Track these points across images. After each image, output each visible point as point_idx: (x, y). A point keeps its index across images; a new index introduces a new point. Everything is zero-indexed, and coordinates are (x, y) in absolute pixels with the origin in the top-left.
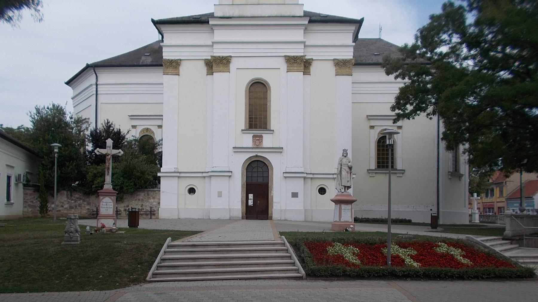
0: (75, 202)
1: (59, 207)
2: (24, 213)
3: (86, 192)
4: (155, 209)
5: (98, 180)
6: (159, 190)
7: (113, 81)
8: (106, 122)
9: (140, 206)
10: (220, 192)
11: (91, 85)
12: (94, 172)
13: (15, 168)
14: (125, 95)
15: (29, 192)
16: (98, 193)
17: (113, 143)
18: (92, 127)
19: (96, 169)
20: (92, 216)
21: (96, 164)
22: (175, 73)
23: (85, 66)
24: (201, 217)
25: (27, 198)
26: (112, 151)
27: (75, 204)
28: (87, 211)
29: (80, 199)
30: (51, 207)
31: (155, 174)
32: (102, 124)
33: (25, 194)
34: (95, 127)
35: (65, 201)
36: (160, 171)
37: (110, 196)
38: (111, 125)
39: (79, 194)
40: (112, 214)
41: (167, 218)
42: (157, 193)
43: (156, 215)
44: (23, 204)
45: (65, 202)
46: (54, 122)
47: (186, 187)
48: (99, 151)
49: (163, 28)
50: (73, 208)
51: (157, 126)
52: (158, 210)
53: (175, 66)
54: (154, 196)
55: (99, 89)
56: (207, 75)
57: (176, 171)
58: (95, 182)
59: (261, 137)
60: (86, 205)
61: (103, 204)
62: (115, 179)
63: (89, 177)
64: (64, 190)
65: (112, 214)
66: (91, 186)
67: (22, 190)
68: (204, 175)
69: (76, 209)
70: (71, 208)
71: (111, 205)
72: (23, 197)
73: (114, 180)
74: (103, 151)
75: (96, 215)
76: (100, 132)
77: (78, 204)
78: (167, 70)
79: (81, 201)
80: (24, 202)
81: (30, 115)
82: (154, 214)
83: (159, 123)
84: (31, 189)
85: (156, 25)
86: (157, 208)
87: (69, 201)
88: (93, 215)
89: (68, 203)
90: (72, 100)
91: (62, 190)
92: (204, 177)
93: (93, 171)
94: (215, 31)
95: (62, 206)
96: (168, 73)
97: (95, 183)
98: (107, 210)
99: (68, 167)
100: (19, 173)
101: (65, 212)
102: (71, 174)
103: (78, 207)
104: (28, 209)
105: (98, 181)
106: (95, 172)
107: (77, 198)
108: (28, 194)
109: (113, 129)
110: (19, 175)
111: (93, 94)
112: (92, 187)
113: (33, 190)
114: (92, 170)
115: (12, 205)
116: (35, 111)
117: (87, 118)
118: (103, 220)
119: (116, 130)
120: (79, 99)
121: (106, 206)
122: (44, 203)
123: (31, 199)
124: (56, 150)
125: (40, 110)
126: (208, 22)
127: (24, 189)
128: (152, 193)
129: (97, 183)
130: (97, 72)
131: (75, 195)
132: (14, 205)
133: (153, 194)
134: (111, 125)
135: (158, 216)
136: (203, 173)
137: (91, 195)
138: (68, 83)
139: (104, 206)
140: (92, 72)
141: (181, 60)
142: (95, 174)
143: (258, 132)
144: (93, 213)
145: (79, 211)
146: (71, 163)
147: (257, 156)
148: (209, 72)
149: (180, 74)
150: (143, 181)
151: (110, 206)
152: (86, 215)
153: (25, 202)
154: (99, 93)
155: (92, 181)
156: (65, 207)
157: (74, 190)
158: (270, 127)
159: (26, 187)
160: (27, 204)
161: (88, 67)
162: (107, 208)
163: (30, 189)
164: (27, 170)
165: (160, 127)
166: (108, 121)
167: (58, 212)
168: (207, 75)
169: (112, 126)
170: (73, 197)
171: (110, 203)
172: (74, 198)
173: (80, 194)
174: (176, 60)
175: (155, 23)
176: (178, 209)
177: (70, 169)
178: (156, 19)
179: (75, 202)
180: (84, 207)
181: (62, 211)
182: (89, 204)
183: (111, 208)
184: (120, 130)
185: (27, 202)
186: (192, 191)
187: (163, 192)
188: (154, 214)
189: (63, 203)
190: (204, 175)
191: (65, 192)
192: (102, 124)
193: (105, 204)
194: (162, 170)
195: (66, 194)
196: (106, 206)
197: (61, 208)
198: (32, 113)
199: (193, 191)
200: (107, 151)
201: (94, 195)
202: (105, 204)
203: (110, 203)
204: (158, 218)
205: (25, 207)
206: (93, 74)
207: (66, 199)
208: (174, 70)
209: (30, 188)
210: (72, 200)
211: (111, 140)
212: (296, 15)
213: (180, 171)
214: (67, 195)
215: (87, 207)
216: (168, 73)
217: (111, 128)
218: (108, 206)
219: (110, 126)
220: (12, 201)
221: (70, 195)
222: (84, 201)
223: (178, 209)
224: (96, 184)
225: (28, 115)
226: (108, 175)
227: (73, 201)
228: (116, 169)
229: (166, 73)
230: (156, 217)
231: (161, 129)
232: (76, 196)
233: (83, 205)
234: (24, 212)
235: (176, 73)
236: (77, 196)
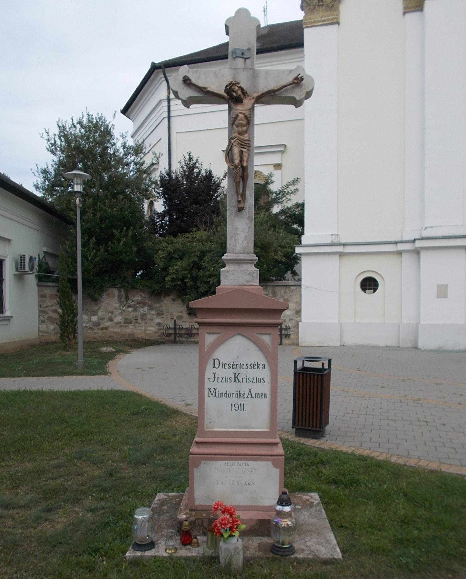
0: (135, 310)
1: (106, 320)
2: (41, 334)
3: (155, 290)
4: (290, 325)
5: (176, 265)
6: (297, 283)
8: (187, 158)
10: (443, 285)
11: (160, 102)
12: (169, 249)
13: (12, 241)
14: (217, 112)
15: (47, 291)
18: (162, 168)
19: (172, 243)
20: (167, 338)
21: (170, 234)
22: (329, 20)
24: (392, 342)
25: (45, 305)
27: (135, 314)
28: (157, 327)
29: (144, 304)
30: (91, 321)
31: (289, 250)
32: (180, 162)
33: (42, 296)
34: (167, 168)
35: (116, 308)
36: (301, 243)
37: (254, 332)
38: (196, 163)
39: (142, 294)
40: (265, 429)
41: (317, 345)
42: (292, 291)
43: (292, 337)
44: (39, 316)
45: (115, 311)
46: (82, 133)
47: (357, 277)
48: (194, 80)
50: (131, 323)
51: (272, 166)
52: (297, 326)
53: (330, 5)
54: (286, 297)
55: (172, 108)
56: (404, 13)
57: (336, 241)
58: (171, 270)
60: (154, 316)
61: (221, 372)
62: (208, 263)
63: (160, 258)
64: (114, 286)
65: (265, 429)
66: (164, 279)
67: (36, 288)
68: (400, 247)
69: (137, 325)
70: (128, 322)
71: (260, 380)
72: (39, 303)
73: (207, 265)
75: (173, 336)
76: (177, 178)
77: (140, 313)
78: (313, 16)
79: (146, 308)
80: (40, 312)
81: (47, 138)
82: (288, 336)
83: (276, 159)
84: (55, 286)
86: (293, 322)
87: (124, 308)
88: (168, 335)
89: (121, 313)
91: (109, 287)
92: (400, 253)
93: (167, 247)
95: (111, 320)
96: (315, 22)
97: (170, 272)
98: (241, 407)
99: (119, 241)
100: (22, 253)
101: (116, 330)
102: (124, 254)
103: (140, 321)
104: (47, 327)
105: (176, 267)
106: (170, 248)
107: (138, 303)
108: (48, 295)
109: (199, 172)
110: (22, 258)
111: (164, 118)
112: (165, 280)
113: (56, 288)
114: (165, 245)
115: (9, 320)
116: (57, 131)
118: (221, 464)
119: (203, 173)
121: (232, 387)
122: (68, 316)
123: (52, 306)
124: (78, 188)
125: (68, 130)
127: (38, 286)
128: (282, 292)
129: (174, 271)
131: (134, 297)
132: (12, 320)
133: (285, 293)
134: (196, 163)
135: (298, 339)
136: (396, 243)
137: (164, 297)
139: (222, 387)
140: (161, 78)
142: (170, 253)
144: (167, 332)
145: (143, 329)
146: (123, 233)
148: (409, 5)
149: (341, 21)
150: (265, 266)
151: (257, 388)
152: (156, 337)
153: (42, 312)
154: (172, 114)
155: (165, 269)
156: (116, 320)
157: (133, 288)
159: (42, 281)
160: (46, 317)
161: (155, 68)
162: (239, 395)
163: (50, 286)
164: (45, 249)
166: (190, 155)
167: (104, 331)
168: (404, 13)
169: (197, 165)
170: (130, 302)
171: (255, 366)
172: (133, 303)
173: (144, 295)
176: (341, 325)
177: (122, 243)
179: (135, 310)
180: (152, 320)
181: (111, 330)
182: (160, 314)
183: (258, 395)
184: (210, 171)
185: (45, 312)
187: (307, 288)
188: (288, 336)
189: (112, 313)
190: (400, 247)
191: (116, 291)
192: (180, 162)
193: (229, 373)
194: (304, 240)
195: (117, 294)
196: (232, 387)
197: (109, 324)
198: (51, 134)
199: (370, 285)
201: (169, 295)
203: (255, 366)
204: (298, 345)
205: (43, 322)
206: (163, 81)
207: (117, 305)
208: (328, 13)
209: (49, 284)
210: (129, 306)
213: (343, 241)
214: (120, 297)
215: (157, 321)
216: (315, 22)
217: (196, 170)
218: (244, 388)
219: (194, 167)
220: (8, 313)
221: (124, 296)
222: (151, 308)
223: (341, 325)
224: (172, 273)
225: (42, 137)
226: (240, 210)
227: (130, 309)
228: (209, 244)
229: (311, 23)
230: (290, 341)
231: (280, 171)
232: (136, 298)
233: (149, 317)
234: (41, 332)
235: (332, 19)
236: (138, 298)
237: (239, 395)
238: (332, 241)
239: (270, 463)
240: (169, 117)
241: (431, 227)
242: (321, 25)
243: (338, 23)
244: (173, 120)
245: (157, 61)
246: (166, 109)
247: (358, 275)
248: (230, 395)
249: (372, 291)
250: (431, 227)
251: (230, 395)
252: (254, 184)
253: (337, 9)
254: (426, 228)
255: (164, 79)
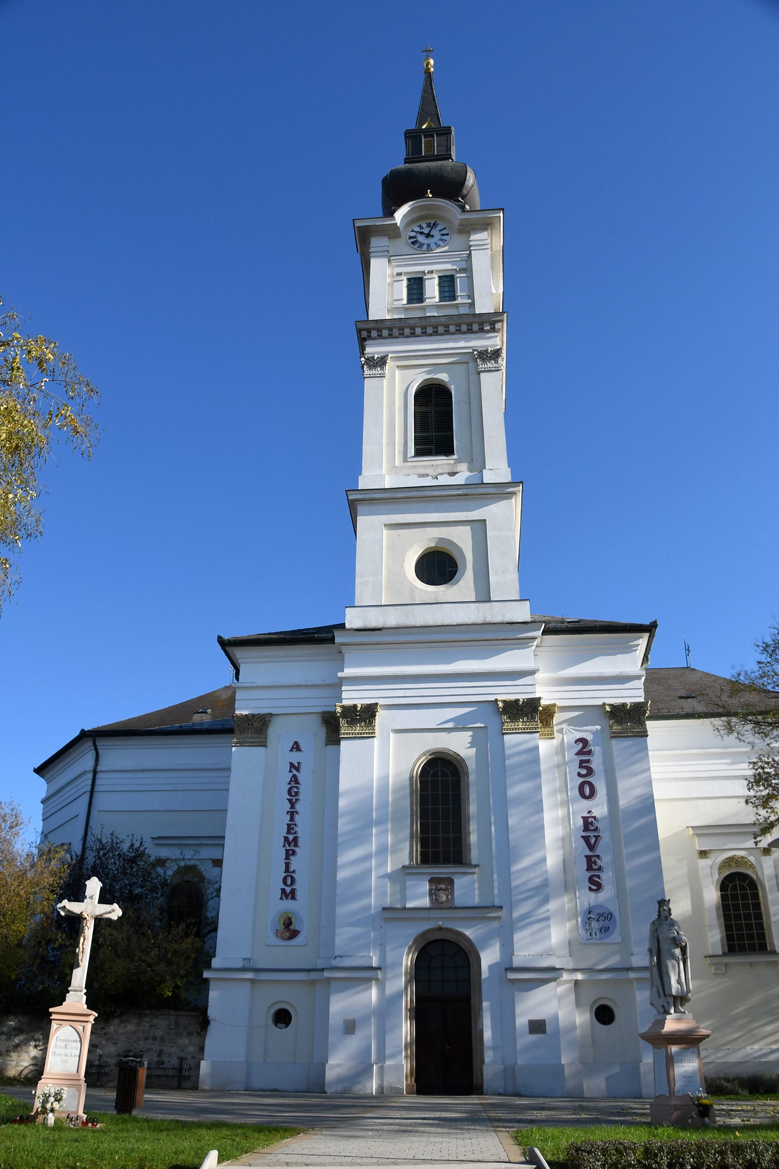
7: (130, 765)
9: (156, 1054)
11: (85, 773)
16: (50, 1014)
17: (101, 888)
23: (76, 733)
26: (95, 906)
37: (73, 1024)
49: (239, 653)
55: (98, 782)
56: (326, 745)
59: (451, 882)
74: (75, 907)
85: (227, 648)
90: (42, 805)
94: (346, 656)
111: (86, 792)
117: (65, 842)
120: (57, 801)
121: (63, 1051)
126: (332, 640)
130: (98, 747)
138: (40, 771)
139: (58, 1051)
141: (271, 715)
143: (442, 871)
147: (440, 929)
154: (97, 789)
158: (470, 860)
161: (84, 735)
162: (66, 1055)
165: (218, 863)
168: (326, 745)
173: (22, 1020)
174: (262, 715)
175: (224, 644)
178: (226, 637)
186: (282, 1017)
193: (63, 1044)
194: (215, 963)
196: (63, 1051)
200: (86, 908)
202: (63, 1044)
211: (98, 880)
212: (515, 620)
237: (66, 1055)
238: (244, 965)
239: (75, 1089)
240: (95, 772)
241: (341, 957)
242: (248, 746)
243: (266, 746)
244: (95, 795)
245: (87, 728)
246: (90, 782)
247: (271, 1006)
248: (62, 1055)
249: (285, 1025)
250: (341, 957)
251: (62, 1055)
252: (377, 735)
253: (265, 733)
254: (336, 957)
255: (93, 748)
